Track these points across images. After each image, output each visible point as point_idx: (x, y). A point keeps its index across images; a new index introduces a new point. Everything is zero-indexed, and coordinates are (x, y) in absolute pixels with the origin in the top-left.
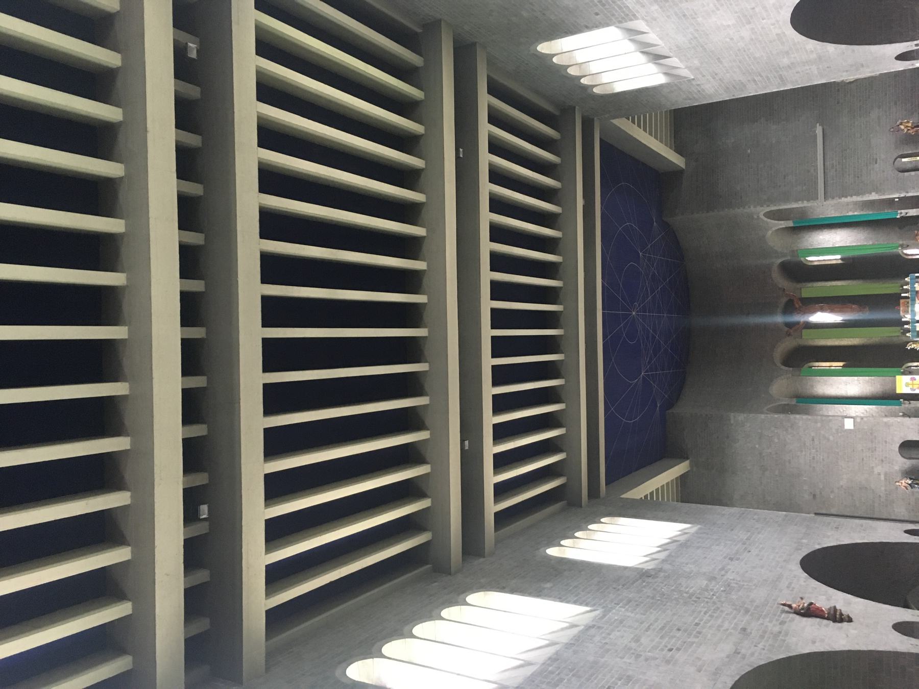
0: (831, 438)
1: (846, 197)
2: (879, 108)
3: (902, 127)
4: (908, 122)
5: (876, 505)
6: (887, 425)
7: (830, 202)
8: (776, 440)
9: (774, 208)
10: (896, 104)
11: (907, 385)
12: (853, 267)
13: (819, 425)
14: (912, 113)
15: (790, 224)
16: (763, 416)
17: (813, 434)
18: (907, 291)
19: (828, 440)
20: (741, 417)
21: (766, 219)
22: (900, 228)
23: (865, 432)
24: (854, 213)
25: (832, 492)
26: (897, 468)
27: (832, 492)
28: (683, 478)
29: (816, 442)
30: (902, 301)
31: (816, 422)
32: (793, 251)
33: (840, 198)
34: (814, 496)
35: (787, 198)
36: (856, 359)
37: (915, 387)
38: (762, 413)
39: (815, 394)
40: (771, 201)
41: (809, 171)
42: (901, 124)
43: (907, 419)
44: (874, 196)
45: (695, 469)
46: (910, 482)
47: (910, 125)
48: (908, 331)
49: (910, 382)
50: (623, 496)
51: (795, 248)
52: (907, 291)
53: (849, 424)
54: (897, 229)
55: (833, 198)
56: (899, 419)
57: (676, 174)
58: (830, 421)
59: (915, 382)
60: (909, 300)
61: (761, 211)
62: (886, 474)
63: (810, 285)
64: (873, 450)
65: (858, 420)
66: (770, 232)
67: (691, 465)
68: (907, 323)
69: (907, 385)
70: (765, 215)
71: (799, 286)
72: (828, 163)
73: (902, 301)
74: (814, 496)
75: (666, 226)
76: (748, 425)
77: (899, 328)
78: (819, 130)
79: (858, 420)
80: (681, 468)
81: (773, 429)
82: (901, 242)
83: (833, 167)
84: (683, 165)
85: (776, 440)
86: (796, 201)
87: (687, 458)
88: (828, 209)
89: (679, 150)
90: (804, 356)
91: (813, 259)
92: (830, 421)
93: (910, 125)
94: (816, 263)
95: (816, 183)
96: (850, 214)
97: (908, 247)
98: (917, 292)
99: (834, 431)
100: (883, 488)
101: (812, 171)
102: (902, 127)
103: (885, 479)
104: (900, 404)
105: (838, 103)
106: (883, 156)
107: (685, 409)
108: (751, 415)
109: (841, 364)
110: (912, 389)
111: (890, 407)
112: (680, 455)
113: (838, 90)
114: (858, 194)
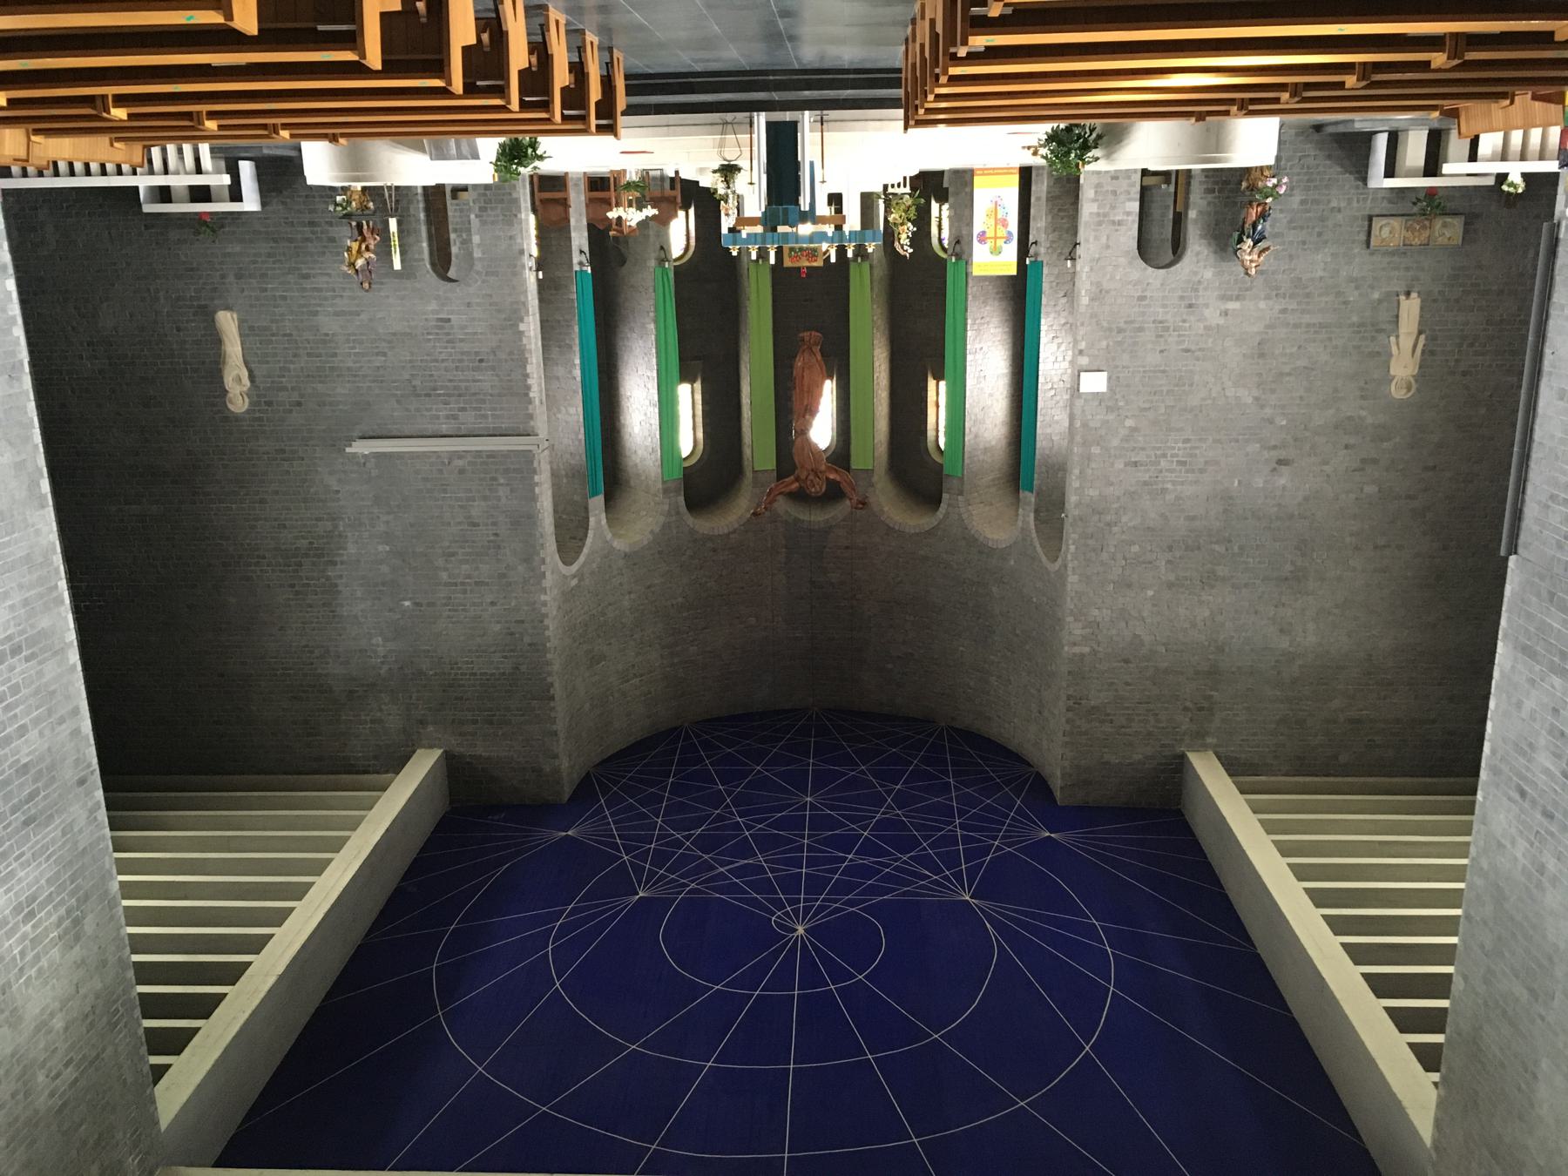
0: (1129, 423)
1: (528, 388)
2: (316, 313)
3: (360, 262)
4: (349, 249)
5: (1307, 319)
6: (1099, 295)
7: (541, 424)
8: (1135, 549)
9: (551, 545)
10: (307, 277)
11: (996, 251)
12: (705, 353)
13: (1095, 450)
14: (332, 240)
15: (597, 502)
16: (1072, 579)
17: (1119, 465)
18: (762, 253)
19: (1134, 429)
20: (1074, 629)
21: (582, 558)
22: (623, 262)
23: (1112, 344)
24: (575, 367)
25: (1271, 421)
26: (1208, 274)
27: (1271, 421)
28: (1234, 767)
29: (1141, 457)
30: (787, 263)
31: (1089, 458)
32: (666, 491)
33: (530, 402)
34: (1280, 462)
35: (525, 521)
36: (923, 350)
37: (1002, 232)
38: (1061, 576)
39: (1004, 442)
40: (530, 556)
41: (462, 471)
42: (352, 265)
43: (1080, 251)
44: (531, 326)
45: (1209, 740)
46: (1250, 242)
47: (355, 246)
48: (860, 251)
49: (990, 244)
50: (1428, 1141)
51: (660, 486)
52: (762, 253)
53: (1095, 383)
54: (624, 270)
55: (531, 417)
56: (1083, 267)
57: (454, 770)
58: (1085, 425)
59: (990, 234)
60: (786, 247)
61: (555, 571)
62: (1225, 298)
63: (747, 452)
64: (1162, 328)
65: (1084, 361)
66: (615, 544)
67: (1204, 747)
68: (841, 251)
69: (996, 251)
70: (567, 563)
71: (749, 474)
72: (444, 428)
73: (787, 263)
74: (1280, 462)
75: (586, 790)
76: (1096, 612)
77: (852, 266)
78: (361, 448)
79: (1084, 361)
80: (1213, 778)
81: (1104, 556)
82: (652, 263)
83: (455, 417)
84: (438, 753)
85: (1135, 549)
86: (533, 498)
87: (1183, 757)
88: (561, 424)
89: (397, 763)
90: (918, 471)
91: (687, 440)
92: (1085, 425)
93: (355, 246)
94: (700, 435)
95: (492, 455)
96: (577, 373)
97: (664, 248)
98: (151, 1173)
99: (1111, 417)
100: (1262, 305)
101: (460, 463)
102: (360, 262)
103: (1238, 298)
104: (1038, 265)
105: (299, 404)
106: (433, 306)
107: (1054, 754)
108: (1070, 605)
109: (931, 383)
110: (1008, 240)
111: (1045, 286)
112: (1177, 772)
113: (269, 404)
114: (523, 363)
